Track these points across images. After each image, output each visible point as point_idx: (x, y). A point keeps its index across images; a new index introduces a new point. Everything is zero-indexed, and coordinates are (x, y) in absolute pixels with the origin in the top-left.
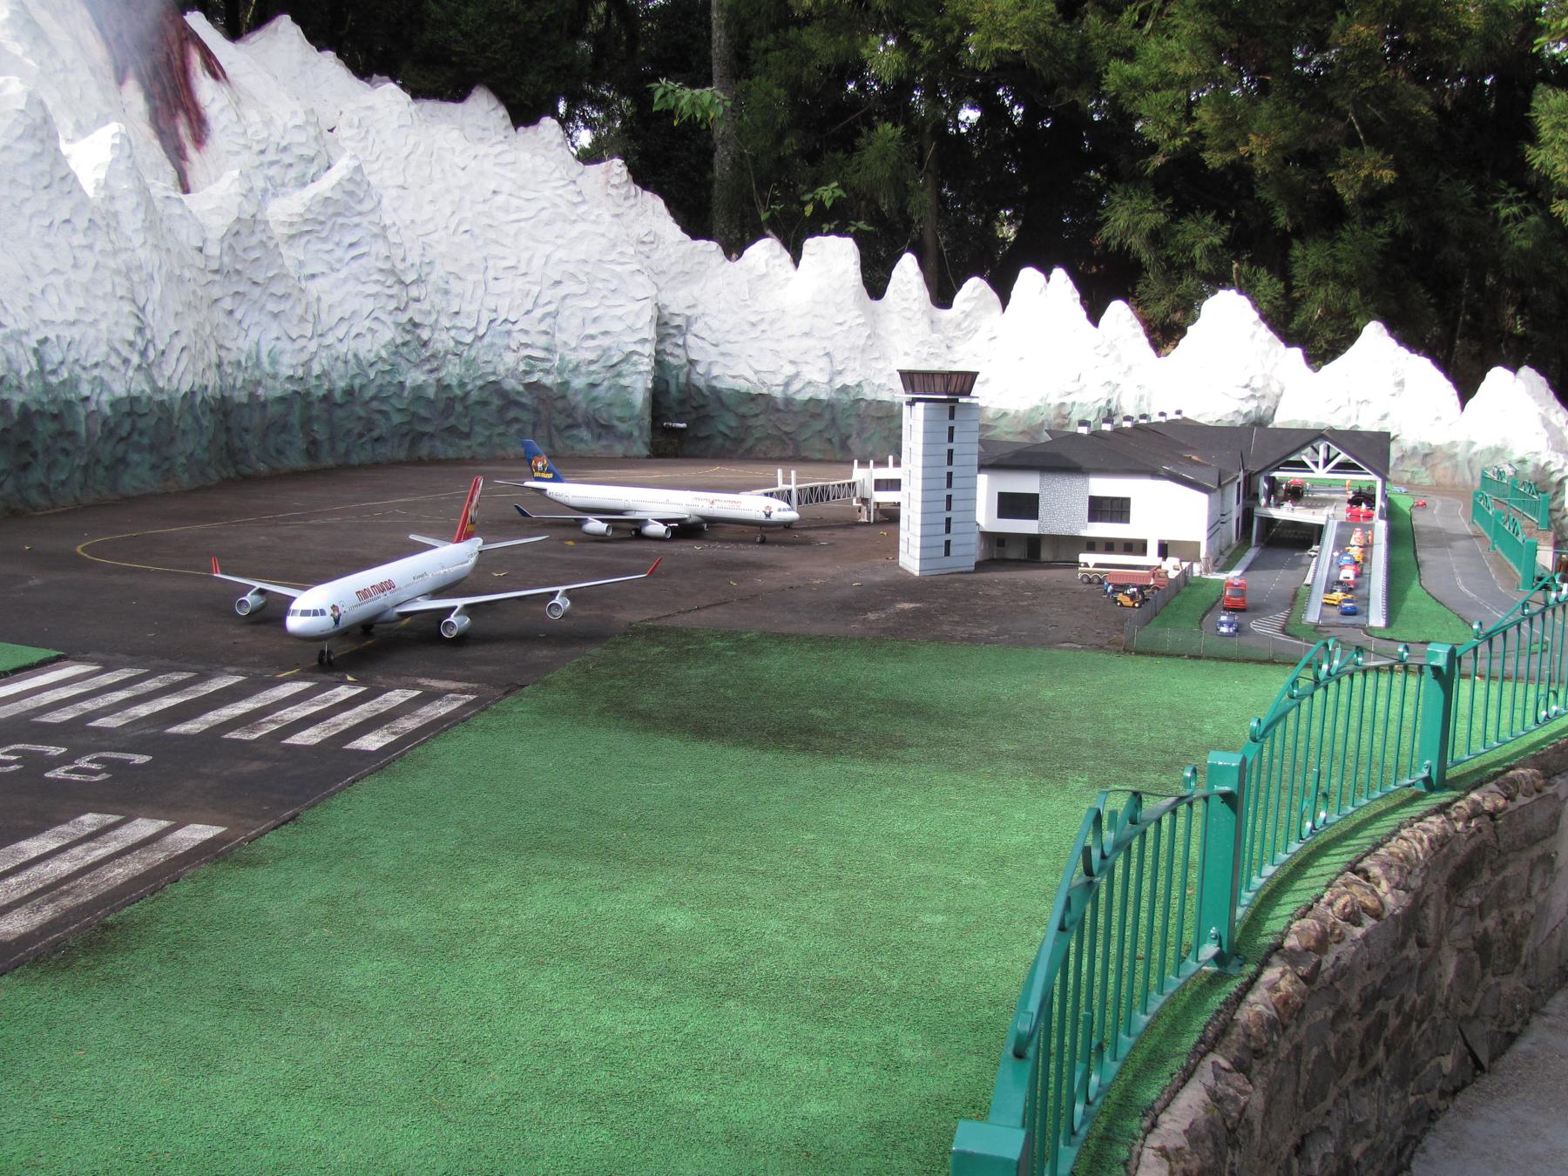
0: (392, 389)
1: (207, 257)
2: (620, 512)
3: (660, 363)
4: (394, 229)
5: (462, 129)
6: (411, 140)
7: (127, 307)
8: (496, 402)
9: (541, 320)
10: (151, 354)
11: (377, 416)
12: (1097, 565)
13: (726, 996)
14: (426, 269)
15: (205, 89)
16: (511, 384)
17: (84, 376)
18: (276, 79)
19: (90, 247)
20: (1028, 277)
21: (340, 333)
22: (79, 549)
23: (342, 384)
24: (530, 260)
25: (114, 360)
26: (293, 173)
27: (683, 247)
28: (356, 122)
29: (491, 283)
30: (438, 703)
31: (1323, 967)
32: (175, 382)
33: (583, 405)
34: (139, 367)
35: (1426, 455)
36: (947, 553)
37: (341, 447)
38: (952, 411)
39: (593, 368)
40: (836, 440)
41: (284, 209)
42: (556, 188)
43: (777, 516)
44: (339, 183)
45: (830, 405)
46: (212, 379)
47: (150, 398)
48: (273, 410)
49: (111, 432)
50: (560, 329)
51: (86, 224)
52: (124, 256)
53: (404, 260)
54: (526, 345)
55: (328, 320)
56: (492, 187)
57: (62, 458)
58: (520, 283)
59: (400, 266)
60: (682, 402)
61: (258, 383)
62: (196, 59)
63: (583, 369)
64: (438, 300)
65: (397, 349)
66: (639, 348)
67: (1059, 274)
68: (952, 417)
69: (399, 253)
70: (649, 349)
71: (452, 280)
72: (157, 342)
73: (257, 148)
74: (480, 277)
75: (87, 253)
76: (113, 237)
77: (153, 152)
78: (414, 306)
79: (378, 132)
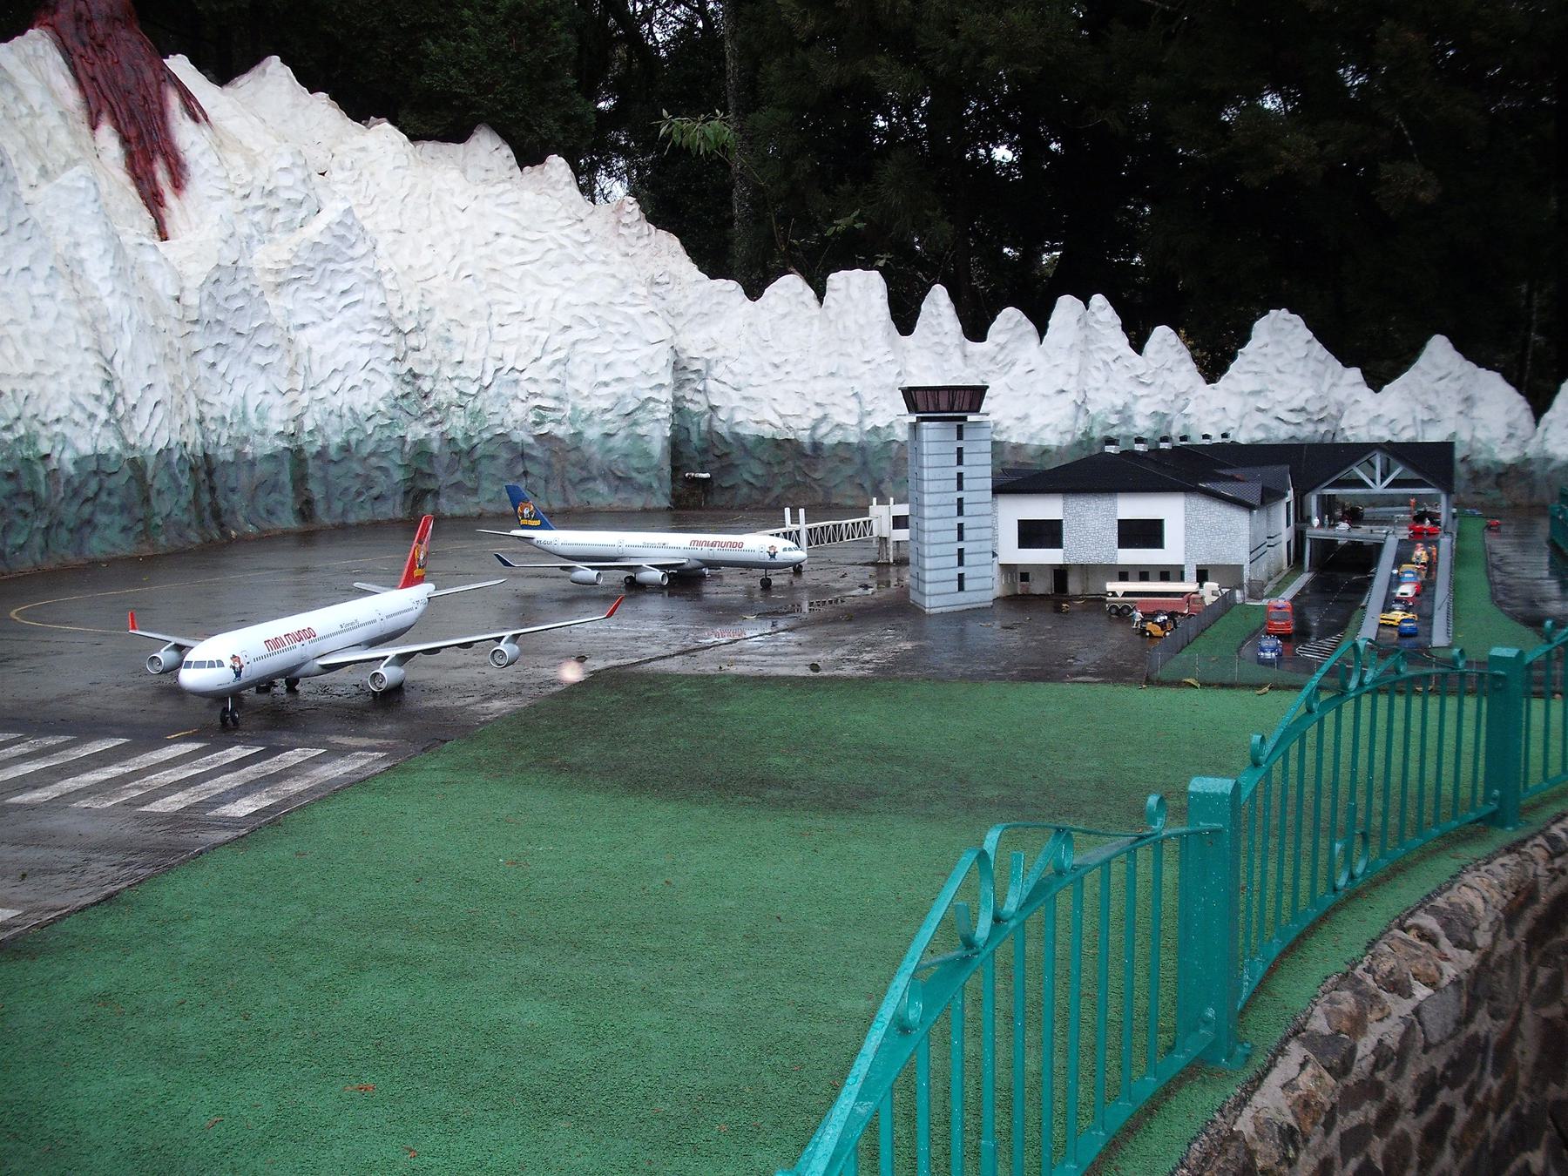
0: (392, 444)
1: (185, 307)
2: (615, 559)
3: (678, 410)
4: (389, 276)
5: (464, 171)
6: (408, 182)
7: (92, 359)
8: (505, 455)
9: (550, 368)
10: (121, 409)
11: (378, 473)
12: (1126, 594)
13: (560, 1113)
14: (426, 317)
15: (185, 133)
16: (520, 436)
17: (43, 432)
18: (261, 127)
19: (52, 296)
20: (1066, 305)
21: (334, 384)
22: (13, 614)
23: (337, 440)
24: (537, 304)
25: (78, 415)
26: (280, 218)
27: (700, 287)
28: (348, 164)
29: (496, 330)
30: (340, 761)
31: (1359, 1055)
32: (148, 438)
33: (599, 457)
34: (107, 422)
35: (1499, 475)
36: (961, 588)
37: (338, 507)
38: (960, 430)
39: (608, 416)
40: (867, 485)
41: (266, 257)
42: (562, 228)
43: (782, 556)
44: (328, 227)
45: (862, 448)
46: (193, 436)
47: (119, 456)
48: (263, 469)
49: (76, 492)
50: (571, 377)
51: (47, 272)
52: (90, 305)
53: (401, 307)
54: (535, 395)
55: (321, 372)
56: (495, 229)
57: (20, 521)
58: (527, 329)
59: (397, 314)
60: (705, 451)
61: (246, 440)
62: (174, 101)
63: (596, 419)
64: (439, 348)
65: (398, 401)
66: (654, 395)
67: (1098, 300)
68: (960, 437)
69: (394, 301)
70: (666, 395)
71: (453, 326)
72: (127, 396)
73: (240, 192)
74: (484, 324)
75: (47, 302)
76: (78, 286)
77: (128, 197)
78: (412, 356)
79: (372, 174)
